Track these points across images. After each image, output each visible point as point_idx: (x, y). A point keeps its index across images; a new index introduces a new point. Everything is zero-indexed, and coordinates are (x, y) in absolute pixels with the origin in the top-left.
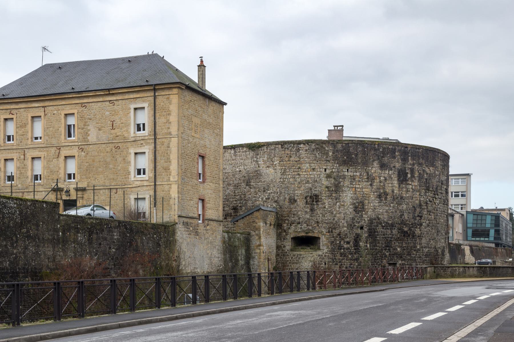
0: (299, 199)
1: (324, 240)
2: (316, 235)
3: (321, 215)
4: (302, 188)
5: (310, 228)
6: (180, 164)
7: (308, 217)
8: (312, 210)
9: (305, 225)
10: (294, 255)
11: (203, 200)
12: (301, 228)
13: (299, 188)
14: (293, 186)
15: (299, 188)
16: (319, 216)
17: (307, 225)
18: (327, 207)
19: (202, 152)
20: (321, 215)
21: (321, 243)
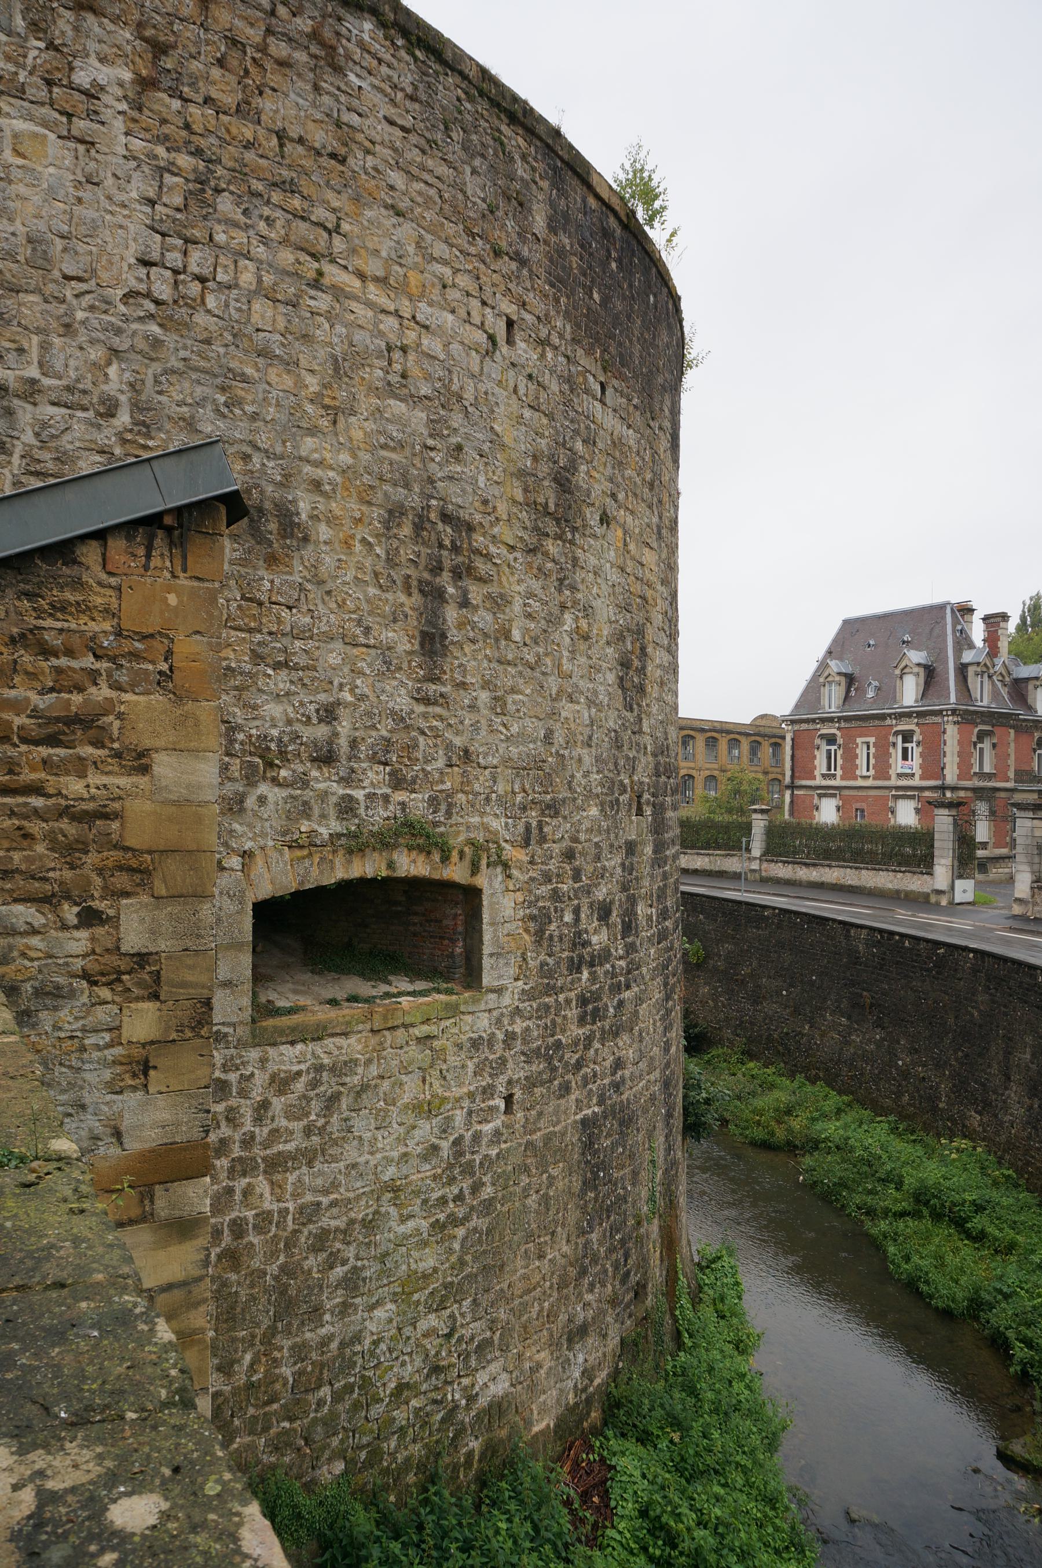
0: (332, 521)
1: (502, 907)
2: (456, 872)
3: (484, 696)
4: (358, 428)
5: (417, 803)
6: (116, 769)
7: (402, 702)
8: (432, 642)
9: (375, 777)
10: (281, 1083)
11: (976, 1471)
12: (347, 808)
13: (334, 413)
14: (280, 379)
15: (334, 413)
16: (473, 707)
17: (397, 782)
18: (516, 635)
19: (975, 1465)
20: (484, 696)
21: (487, 937)
